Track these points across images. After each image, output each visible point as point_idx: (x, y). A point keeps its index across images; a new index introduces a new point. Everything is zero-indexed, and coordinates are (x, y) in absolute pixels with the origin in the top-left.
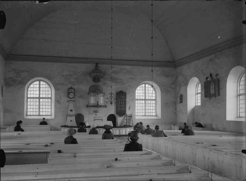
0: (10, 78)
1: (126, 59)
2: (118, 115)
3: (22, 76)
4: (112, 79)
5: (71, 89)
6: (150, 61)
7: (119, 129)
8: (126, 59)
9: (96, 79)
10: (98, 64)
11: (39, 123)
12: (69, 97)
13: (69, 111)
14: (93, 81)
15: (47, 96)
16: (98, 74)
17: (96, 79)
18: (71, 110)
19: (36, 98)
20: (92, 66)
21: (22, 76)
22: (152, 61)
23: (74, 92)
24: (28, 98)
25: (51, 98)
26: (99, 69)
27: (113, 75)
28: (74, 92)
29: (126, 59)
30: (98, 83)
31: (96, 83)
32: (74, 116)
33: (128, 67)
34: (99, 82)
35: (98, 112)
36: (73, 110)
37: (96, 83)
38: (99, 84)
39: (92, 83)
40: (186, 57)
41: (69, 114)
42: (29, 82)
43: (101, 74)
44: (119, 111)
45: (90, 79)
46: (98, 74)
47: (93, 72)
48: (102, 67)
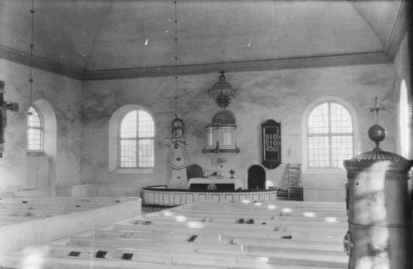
0: (89, 109)
1: (279, 56)
2: (267, 167)
3: (105, 104)
4: (254, 100)
6: (275, 60)
7: (219, 195)
8: (278, 58)
10: (224, 72)
13: (175, 159)
14: (219, 105)
15: (321, 132)
16: (224, 91)
17: (223, 101)
18: (179, 159)
19: (336, 135)
20: (213, 77)
21: (105, 104)
23: (182, 126)
24: (352, 134)
25: (309, 136)
26: (225, 81)
27: (257, 91)
28: (182, 126)
29: (279, 56)
31: (225, 108)
32: (186, 168)
33: (284, 73)
35: (226, 162)
36: (181, 159)
38: (227, 108)
40: (213, 64)
41: (174, 165)
43: (229, 92)
45: (212, 101)
46: (224, 91)
47: (215, 87)
48: (233, 78)
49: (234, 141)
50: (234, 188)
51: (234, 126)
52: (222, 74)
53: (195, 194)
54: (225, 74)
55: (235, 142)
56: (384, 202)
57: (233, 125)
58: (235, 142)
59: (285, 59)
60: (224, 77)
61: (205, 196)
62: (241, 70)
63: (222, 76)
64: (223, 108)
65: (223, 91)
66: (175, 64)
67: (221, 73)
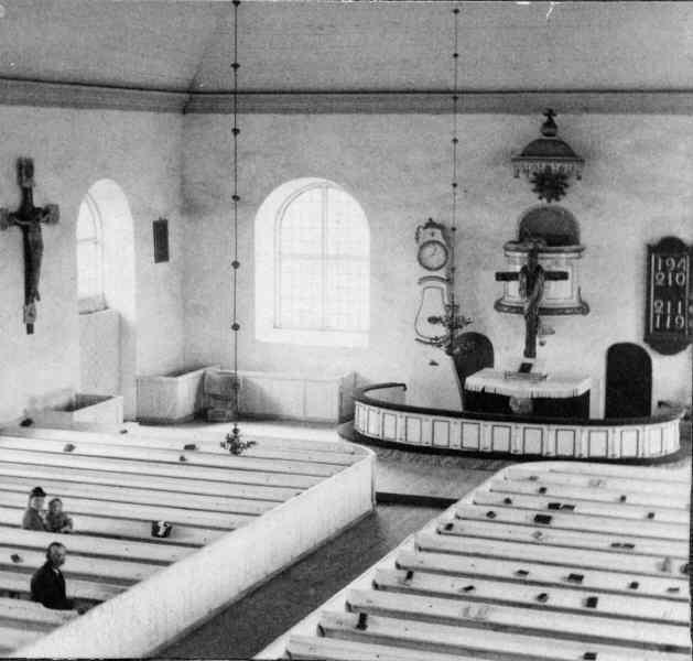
1: (456, 86)
5: (429, 230)
9: (550, 185)
11: (20, 422)
12: (421, 263)
17: (550, 185)
20: (528, 127)
22: (235, 92)
23: (443, 242)
28: (443, 242)
29: (456, 86)
30: (558, 199)
31: (549, 201)
34: (564, 194)
35: (553, 333)
37: (549, 201)
39: (534, 201)
42: (281, 188)
44: (655, 329)
48: (578, 128)
49: (576, 287)
50: (588, 414)
51: (575, 251)
52: (550, 118)
53: (614, 432)
54: (555, 119)
55: (579, 290)
56: (654, 456)
57: (574, 247)
58: (579, 290)
59: (331, 93)
60: (555, 127)
61: (446, 424)
62: (600, 110)
63: (550, 124)
64: (545, 200)
65: (552, 165)
66: (230, 86)
67: (546, 115)
